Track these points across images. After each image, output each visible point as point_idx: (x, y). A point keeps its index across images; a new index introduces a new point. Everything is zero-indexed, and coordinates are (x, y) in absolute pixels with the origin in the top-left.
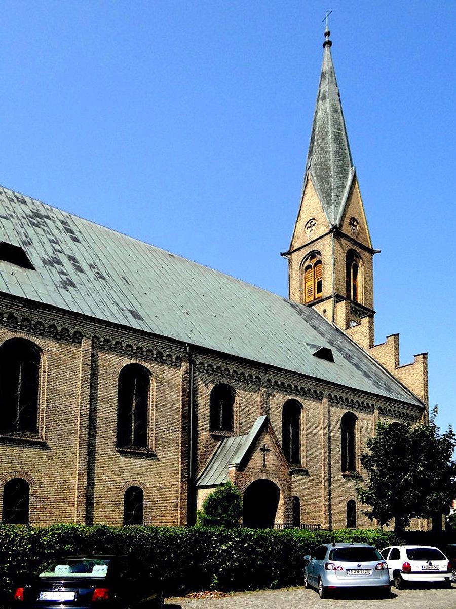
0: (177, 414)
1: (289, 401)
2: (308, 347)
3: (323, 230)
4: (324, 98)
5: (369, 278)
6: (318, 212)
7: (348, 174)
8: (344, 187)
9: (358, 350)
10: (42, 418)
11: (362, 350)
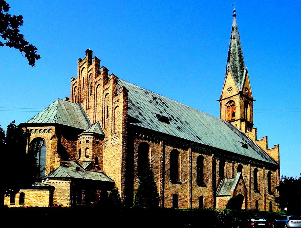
0: (211, 171)
1: (239, 165)
2: (239, 143)
3: (235, 93)
4: (234, 38)
5: (252, 111)
6: (233, 85)
7: (244, 70)
8: (243, 75)
9: (251, 141)
10: (180, 174)
11: (253, 141)
